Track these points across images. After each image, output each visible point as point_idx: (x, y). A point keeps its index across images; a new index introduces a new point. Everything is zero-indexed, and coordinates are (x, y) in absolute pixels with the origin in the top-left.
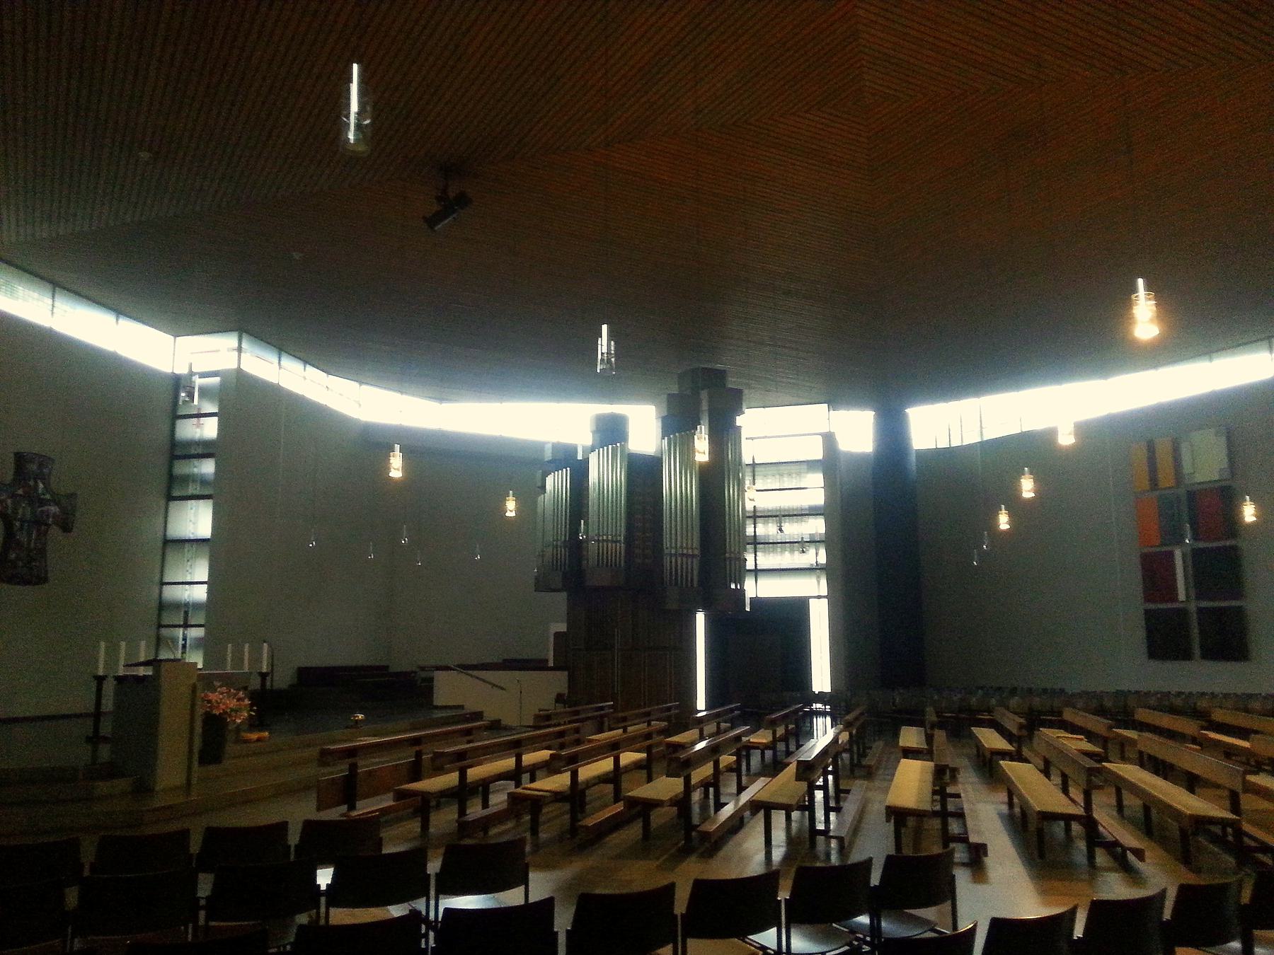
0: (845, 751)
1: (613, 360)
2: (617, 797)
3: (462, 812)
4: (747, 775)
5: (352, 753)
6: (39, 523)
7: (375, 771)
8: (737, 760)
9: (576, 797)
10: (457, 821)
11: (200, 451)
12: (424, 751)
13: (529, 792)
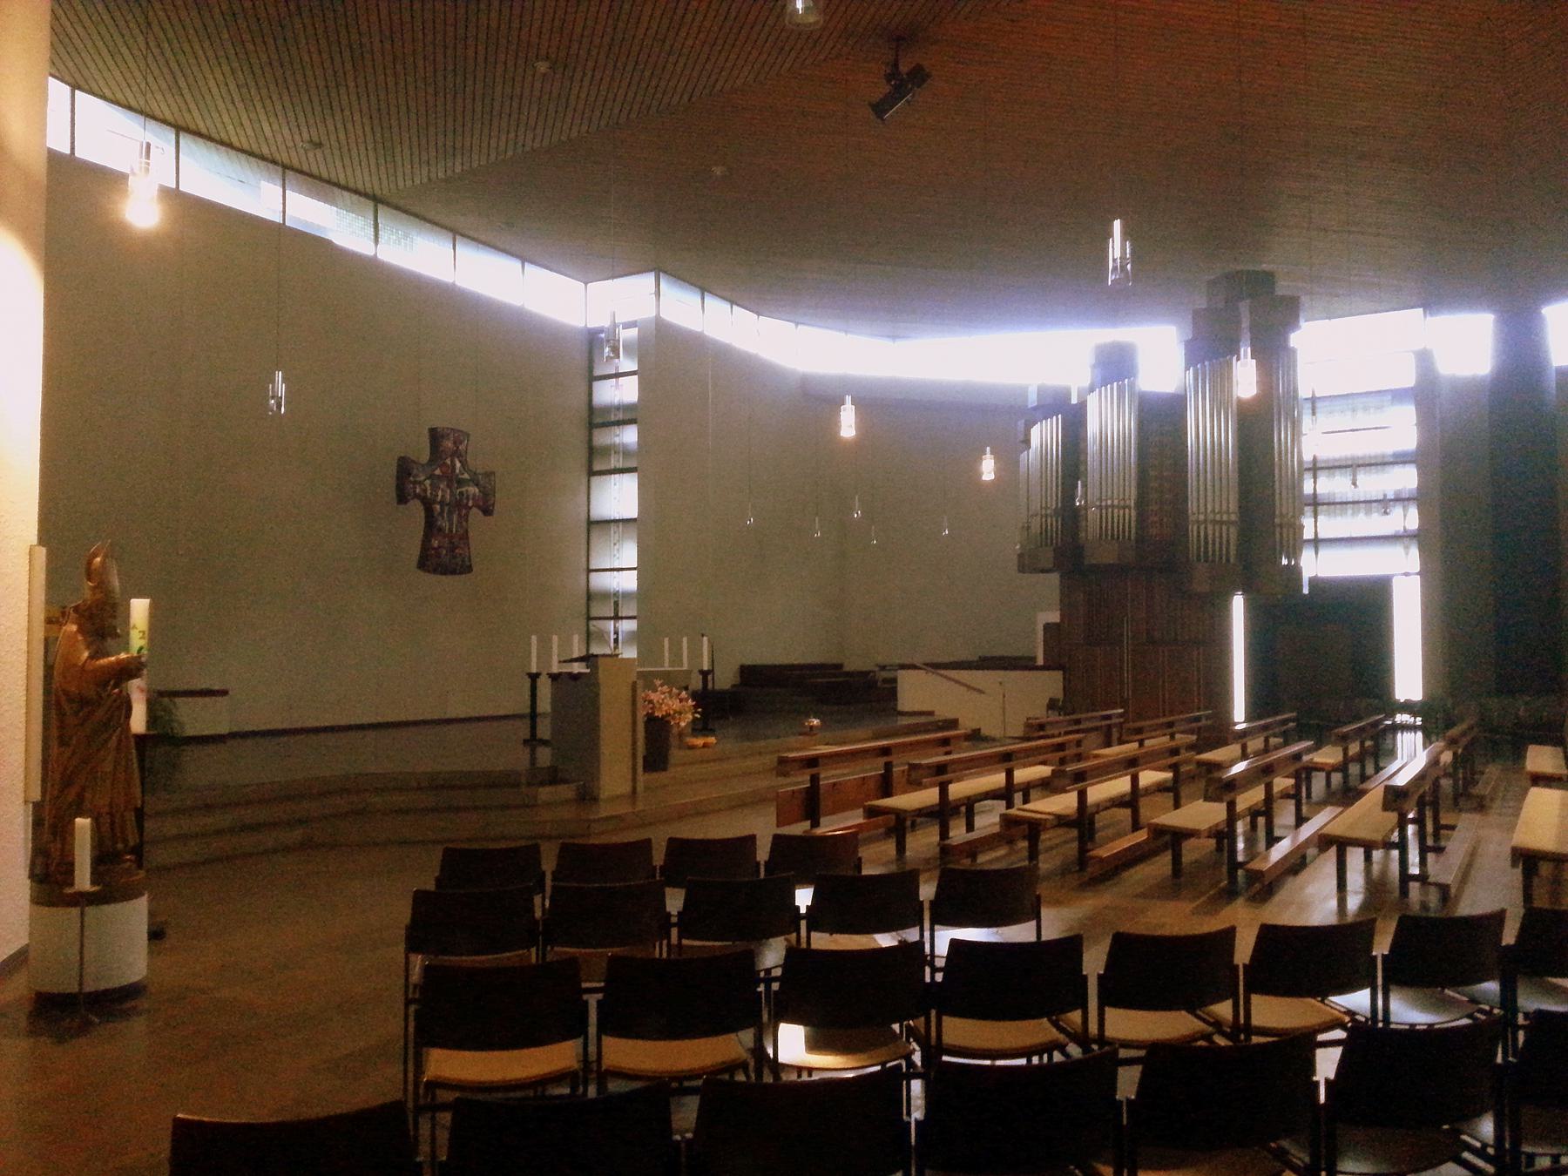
0: (1446, 775)
1: (1129, 266)
2: (1136, 826)
3: (944, 834)
4: (1307, 803)
5: (812, 762)
6: (459, 505)
7: (840, 783)
8: (1296, 783)
9: (1083, 822)
10: (939, 844)
11: (620, 416)
12: (894, 763)
13: (1029, 814)
